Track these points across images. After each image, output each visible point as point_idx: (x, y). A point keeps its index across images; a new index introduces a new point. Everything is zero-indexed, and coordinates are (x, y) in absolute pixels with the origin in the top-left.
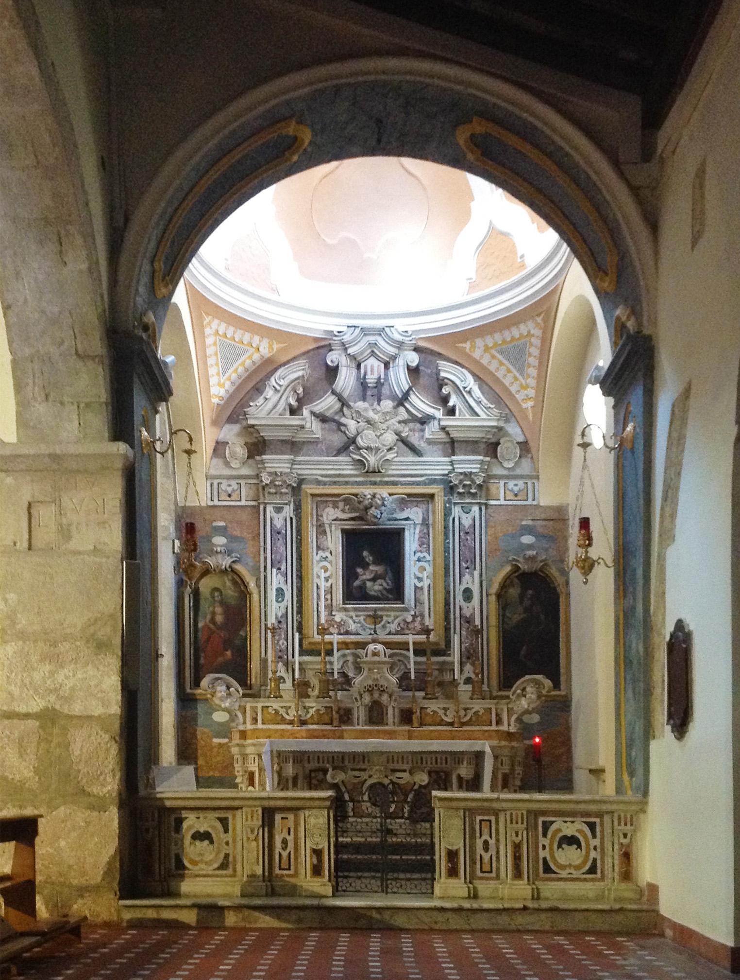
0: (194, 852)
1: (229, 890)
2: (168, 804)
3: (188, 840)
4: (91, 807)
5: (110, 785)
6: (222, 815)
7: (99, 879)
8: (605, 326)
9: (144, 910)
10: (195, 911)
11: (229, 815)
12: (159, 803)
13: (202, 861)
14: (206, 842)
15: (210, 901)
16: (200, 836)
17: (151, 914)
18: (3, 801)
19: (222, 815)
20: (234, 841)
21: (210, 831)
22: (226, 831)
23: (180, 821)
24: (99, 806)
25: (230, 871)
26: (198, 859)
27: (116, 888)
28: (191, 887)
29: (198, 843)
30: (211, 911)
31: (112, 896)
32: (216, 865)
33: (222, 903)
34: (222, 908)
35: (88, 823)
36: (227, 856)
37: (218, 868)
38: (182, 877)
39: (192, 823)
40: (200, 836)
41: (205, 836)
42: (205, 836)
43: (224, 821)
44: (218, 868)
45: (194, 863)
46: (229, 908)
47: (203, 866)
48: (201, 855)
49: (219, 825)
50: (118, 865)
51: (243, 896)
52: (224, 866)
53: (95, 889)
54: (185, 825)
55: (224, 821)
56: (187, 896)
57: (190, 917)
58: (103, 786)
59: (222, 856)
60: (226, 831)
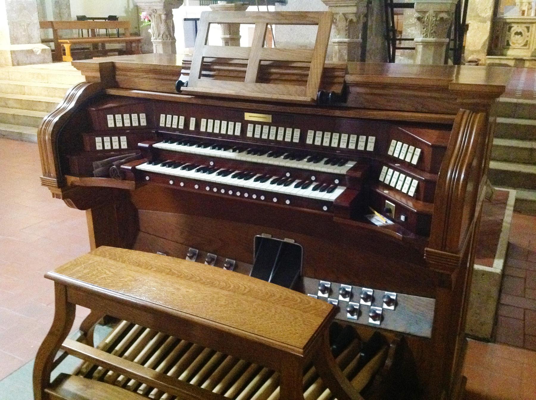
0: (514, 39)
1: (526, 54)
2: (508, 21)
3: (513, 34)
4: (480, 21)
5: (489, 13)
6: (528, 25)
7: (480, 48)
8: (487, 270)
9: (495, 60)
10: (514, 61)
11: (530, 25)
12: (504, 21)
13: (517, 43)
14: (520, 36)
15: (520, 57)
16: (517, 33)
17: (497, 61)
18: (12, 2)
19: (528, 25)
20: (531, 36)
21: (522, 31)
22: (528, 32)
23: (510, 28)
24: (484, 21)
25: (527, 47)
26: (515, 42)
27: (486, 51)
28: (511, 53)
29: (516, 36)
30: (520, 61)
31: (484, 54)
32: (522, 45)
33: (524, 58)
34: (524, 60)
35: (478, 27)
36: (527, 41)
37: (523, 46)
38: (508, 49)
39: (515, 28)
40: (517, 33)
41: (520, 34)
42: (520, 34)
43: (528, 28)
44: (523, 46)
45: (514, 43)
46: (527, 60)
47: (517, 45)
48: (517, 40)
49: (526, 29)
50: (487, 43)
51: (531, 56)
52: (525, 45)
53: (478, 52)
54: (512, 29)
55: (528, 28)
56: (510, 56)
57: (512, 63)
58: (486, 13)
59: (525, 41)
60: (528, 32)
